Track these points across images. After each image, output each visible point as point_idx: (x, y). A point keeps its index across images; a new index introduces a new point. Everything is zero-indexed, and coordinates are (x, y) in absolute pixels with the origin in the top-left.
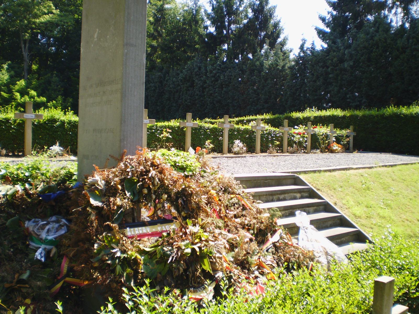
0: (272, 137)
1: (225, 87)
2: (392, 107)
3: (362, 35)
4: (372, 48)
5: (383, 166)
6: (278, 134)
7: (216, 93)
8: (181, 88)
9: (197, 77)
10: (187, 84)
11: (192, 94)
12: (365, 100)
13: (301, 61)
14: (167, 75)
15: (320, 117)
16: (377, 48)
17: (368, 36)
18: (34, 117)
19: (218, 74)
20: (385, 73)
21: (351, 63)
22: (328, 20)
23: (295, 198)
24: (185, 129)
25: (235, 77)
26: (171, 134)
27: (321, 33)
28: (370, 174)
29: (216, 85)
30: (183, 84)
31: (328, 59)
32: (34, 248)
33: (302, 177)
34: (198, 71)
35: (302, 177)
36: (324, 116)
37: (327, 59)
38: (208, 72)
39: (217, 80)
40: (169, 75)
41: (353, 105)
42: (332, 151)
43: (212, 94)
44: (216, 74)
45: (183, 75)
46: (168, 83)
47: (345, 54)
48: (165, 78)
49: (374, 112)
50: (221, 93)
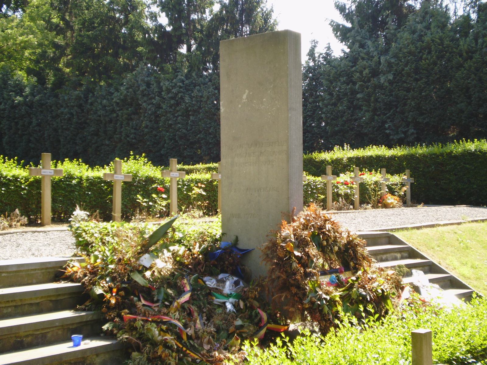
0: (312, 189)
1: (193, 115)
2: (462, 141)
3: (406, 35)
4: (421, 54)
5: (472, 221)
6: (319, 185)
7: (179, 123)
8: (118, 116)
9: (145, 99)
10: (127, 109)
11: (137, 125)
12: (413, 130)
13: (310, 75)
14: (91, 95)
15: (358, 159)
16: (429, 53)
17: (415, 36)
18: (53, 174)
19: (180, 95)
20: (442, 90)
21: (391, 77)
22: (348, 9)
23: (396, 259)
24: (215, 183)
25: (208, 98)
26: (205, 190)
27: (338, 30)
28: (463, 230)
29: (178, 111)
30: (122, 109)
31: (356, 71)
32: (219, 304)
33: (397, 235)
34: (145, 89)
35: (398, 235)
36: (363, 157)
37: (353, 71)
38: (162, 91)
39: (178, 104)
40: (94, 95)
41: (395, 138)
42: (386, 206)
43: (171, 125)
44: (176, 94)
45: (121, 94)
46: (94, 108)
47: (380, 63)
48: (87, 100)
49: (436, 149)
50: (187, 123)
